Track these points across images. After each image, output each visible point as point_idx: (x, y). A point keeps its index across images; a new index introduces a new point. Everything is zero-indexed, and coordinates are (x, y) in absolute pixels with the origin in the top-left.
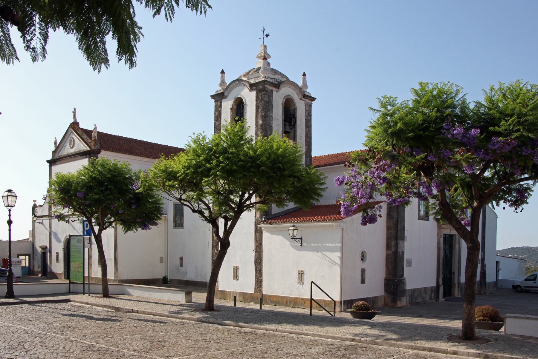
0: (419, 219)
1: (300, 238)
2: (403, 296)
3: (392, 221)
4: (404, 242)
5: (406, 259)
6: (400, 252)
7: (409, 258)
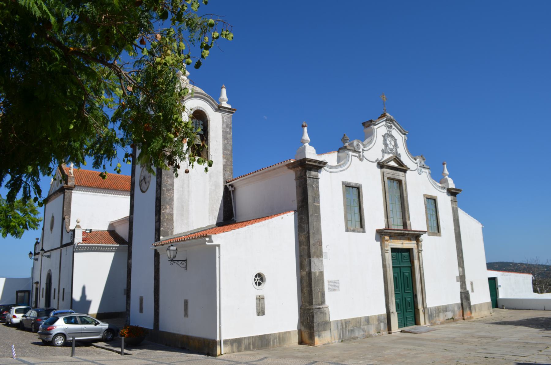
0: (347, 230)
1: (185, 259)
2: (325, 330)
3: (303, 234)
4: (322, 260)
5: (329, 282)
6: (315, 273)
7: (334, 279)
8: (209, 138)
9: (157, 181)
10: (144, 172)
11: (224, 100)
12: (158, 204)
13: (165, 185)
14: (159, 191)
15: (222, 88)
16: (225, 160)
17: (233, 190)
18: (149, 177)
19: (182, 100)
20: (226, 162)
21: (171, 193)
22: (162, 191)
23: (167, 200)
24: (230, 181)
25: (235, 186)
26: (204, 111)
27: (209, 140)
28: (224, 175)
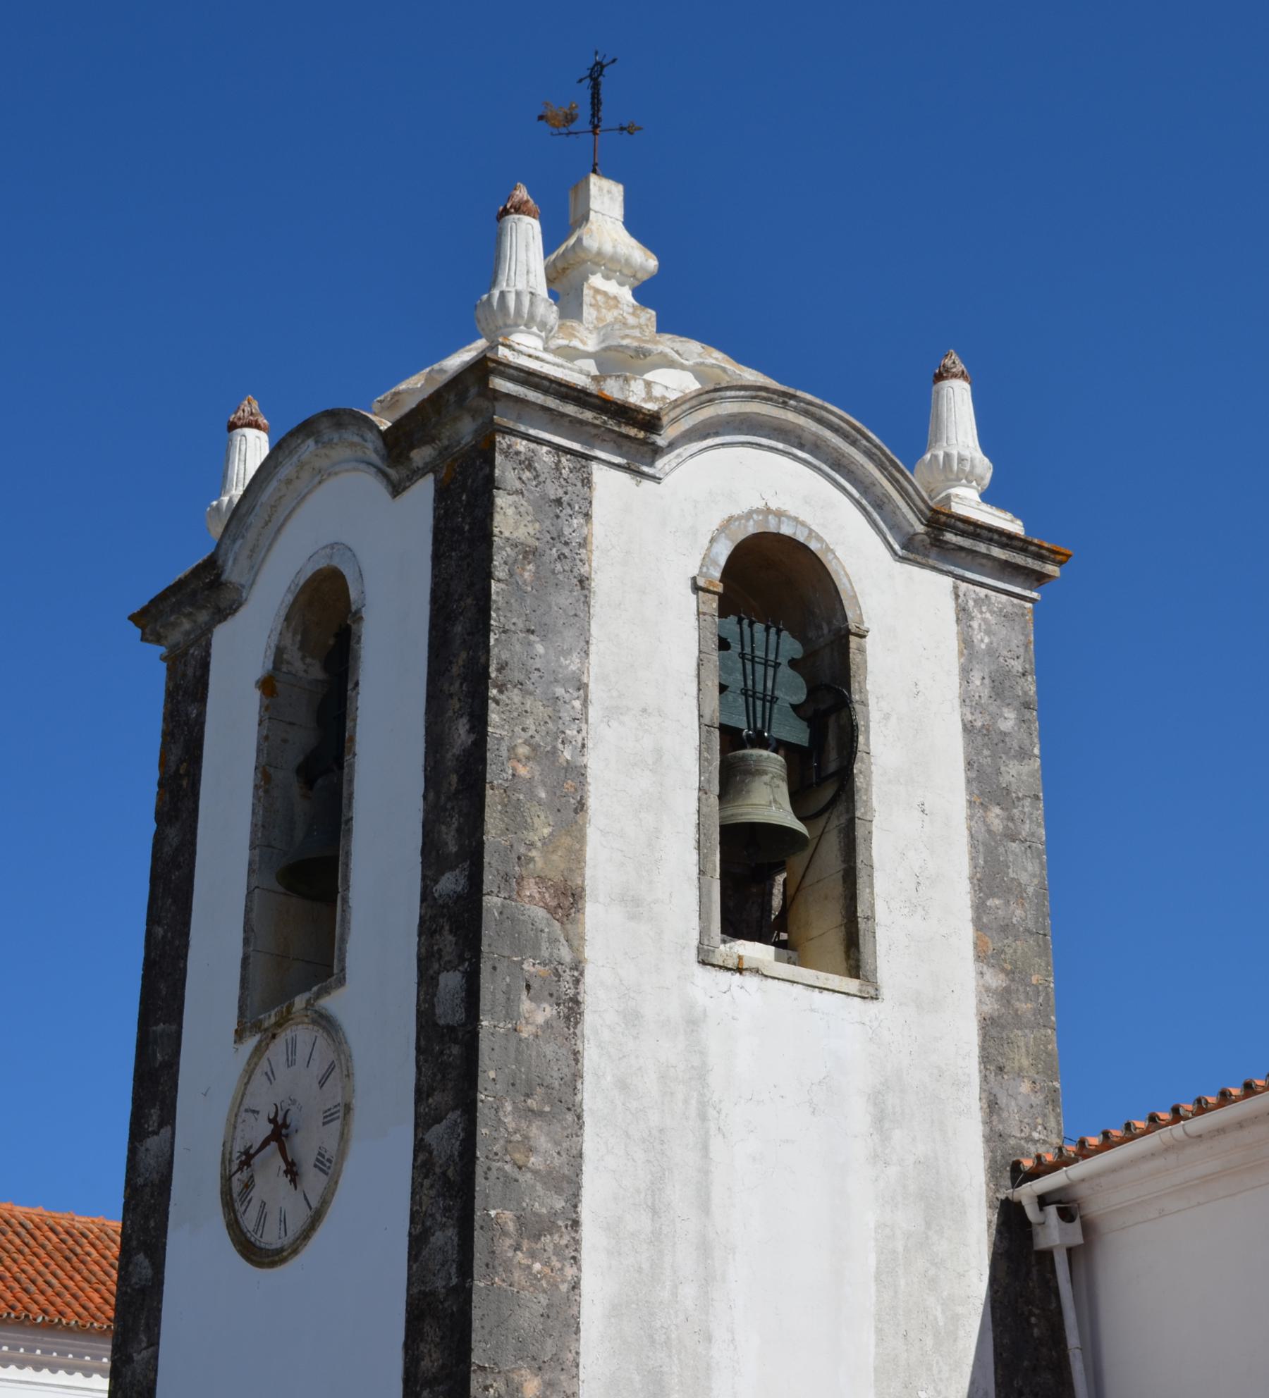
8: (859, 781)
9: (420, 1146)
10: (270, 1076)
11: (969, 478)
12: (431, 1362)
13: (509, 1181)
14: (445, 1237)
15: (939, 377)
16: (996, 980)
17: (1078, 1239)
18: (328, 1118)
19: (644, 442)
20: (1005, 996)
21: (558, 1250)
22: (479, 1238)
23: (526, 1318)
24: (1049, 1157)
25: (1096, 1206)
26: (814, 546)
27: (860, 798)
28: (992, 1106)
